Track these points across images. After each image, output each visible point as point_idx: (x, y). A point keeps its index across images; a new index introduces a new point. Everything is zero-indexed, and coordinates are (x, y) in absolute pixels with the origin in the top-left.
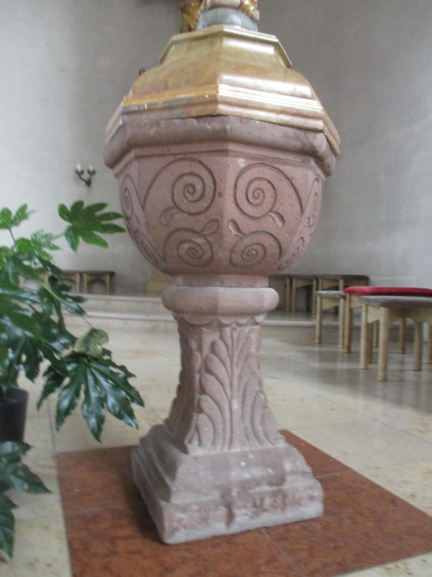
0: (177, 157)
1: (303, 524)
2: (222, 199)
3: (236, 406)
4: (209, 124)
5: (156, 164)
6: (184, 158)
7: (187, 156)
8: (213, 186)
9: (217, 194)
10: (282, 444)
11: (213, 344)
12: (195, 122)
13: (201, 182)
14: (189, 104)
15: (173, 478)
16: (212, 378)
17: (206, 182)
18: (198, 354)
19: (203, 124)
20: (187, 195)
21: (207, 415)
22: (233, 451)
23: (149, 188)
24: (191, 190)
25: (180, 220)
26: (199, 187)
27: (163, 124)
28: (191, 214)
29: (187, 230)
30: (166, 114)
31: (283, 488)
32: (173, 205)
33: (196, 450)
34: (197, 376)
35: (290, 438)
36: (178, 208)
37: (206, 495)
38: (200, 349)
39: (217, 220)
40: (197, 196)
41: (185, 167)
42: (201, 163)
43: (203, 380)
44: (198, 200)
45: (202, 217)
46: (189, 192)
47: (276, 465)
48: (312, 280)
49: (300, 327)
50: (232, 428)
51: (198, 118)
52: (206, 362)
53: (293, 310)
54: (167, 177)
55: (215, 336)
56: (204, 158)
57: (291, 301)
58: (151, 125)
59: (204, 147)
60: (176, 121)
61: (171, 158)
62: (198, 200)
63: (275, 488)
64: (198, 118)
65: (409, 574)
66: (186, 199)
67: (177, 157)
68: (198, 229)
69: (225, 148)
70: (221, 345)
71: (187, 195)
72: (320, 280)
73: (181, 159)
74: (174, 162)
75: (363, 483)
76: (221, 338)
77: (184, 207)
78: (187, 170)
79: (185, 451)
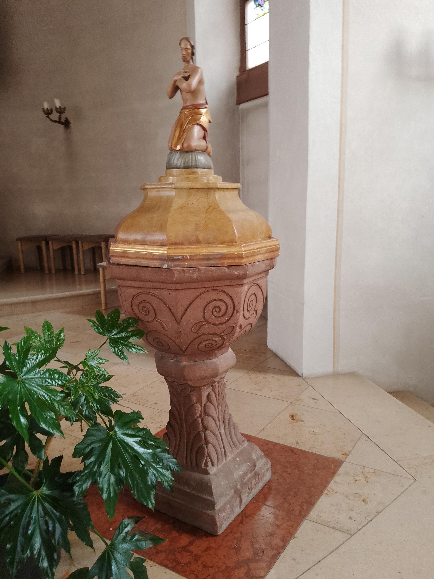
0: (208, 289)
1: (266, 486)
2: (238, 314)
3: (223, 431)
4: (236, 271)
5: (193, 294)
6: (213, 289)
7: (215, 288)
8: (232, 307)
9: (235, 311)
10: (246, 444)
11: (209, 395)
12: (226, 269)
13: (224, 305)
14: (223, 257)
15: (211, 493)
16: (210, 419)
17: (228, 304)
18: (199, 405)
19: (232, 271)
20: (215, 313)
21: (211, 444)
22: (228, 460)
23: (186, 310)
24: (218, 310)
25: (207, 328)
26: (223, 308)
27: (203, 270)
28: (215, 325)
29: (210, 334)
30: (204, 263)
31: (256, 470)
32: (203, 320)
33: (213, 470)
34: (200, 420)
35: (249, 438)
36: (207, 321)
37: (229, 495)
38: (199, 401)
39: (233, 327)
40: (221, 314)
41: (213, 295)
42: (224, 292)
43: (205, 421)
44: (222, 316)
45: (224, 326)
46: (216, 311)
47: (250, 459)
48: (71, 242)
49: (82, 295)
50: (224, 446)
51: (228, 267)
52: (205, 408)
53: (53, 272)
54: (200, 303)
55: (210, 390)
56: (226, 289)
57: (49, 261)
58: (194, 271)
59: (227, 283)
60: (213, 268)
61: (204, 290)
62: (222, 316)
63: (253, 473)
64: (228, 267)
65: (336, 492)
66: (214, 316)
67: (208, 289)
68: (218, 333)
69: (242, 283)
70: (213, 394)
71: (215, 313)
72: (80, 242)
73: (210, 290)
74: (205, 292)
75: (267, 444)
76: (213, 390)
77: (211, 321)
78: (215, 297)
79: (207, 473)
